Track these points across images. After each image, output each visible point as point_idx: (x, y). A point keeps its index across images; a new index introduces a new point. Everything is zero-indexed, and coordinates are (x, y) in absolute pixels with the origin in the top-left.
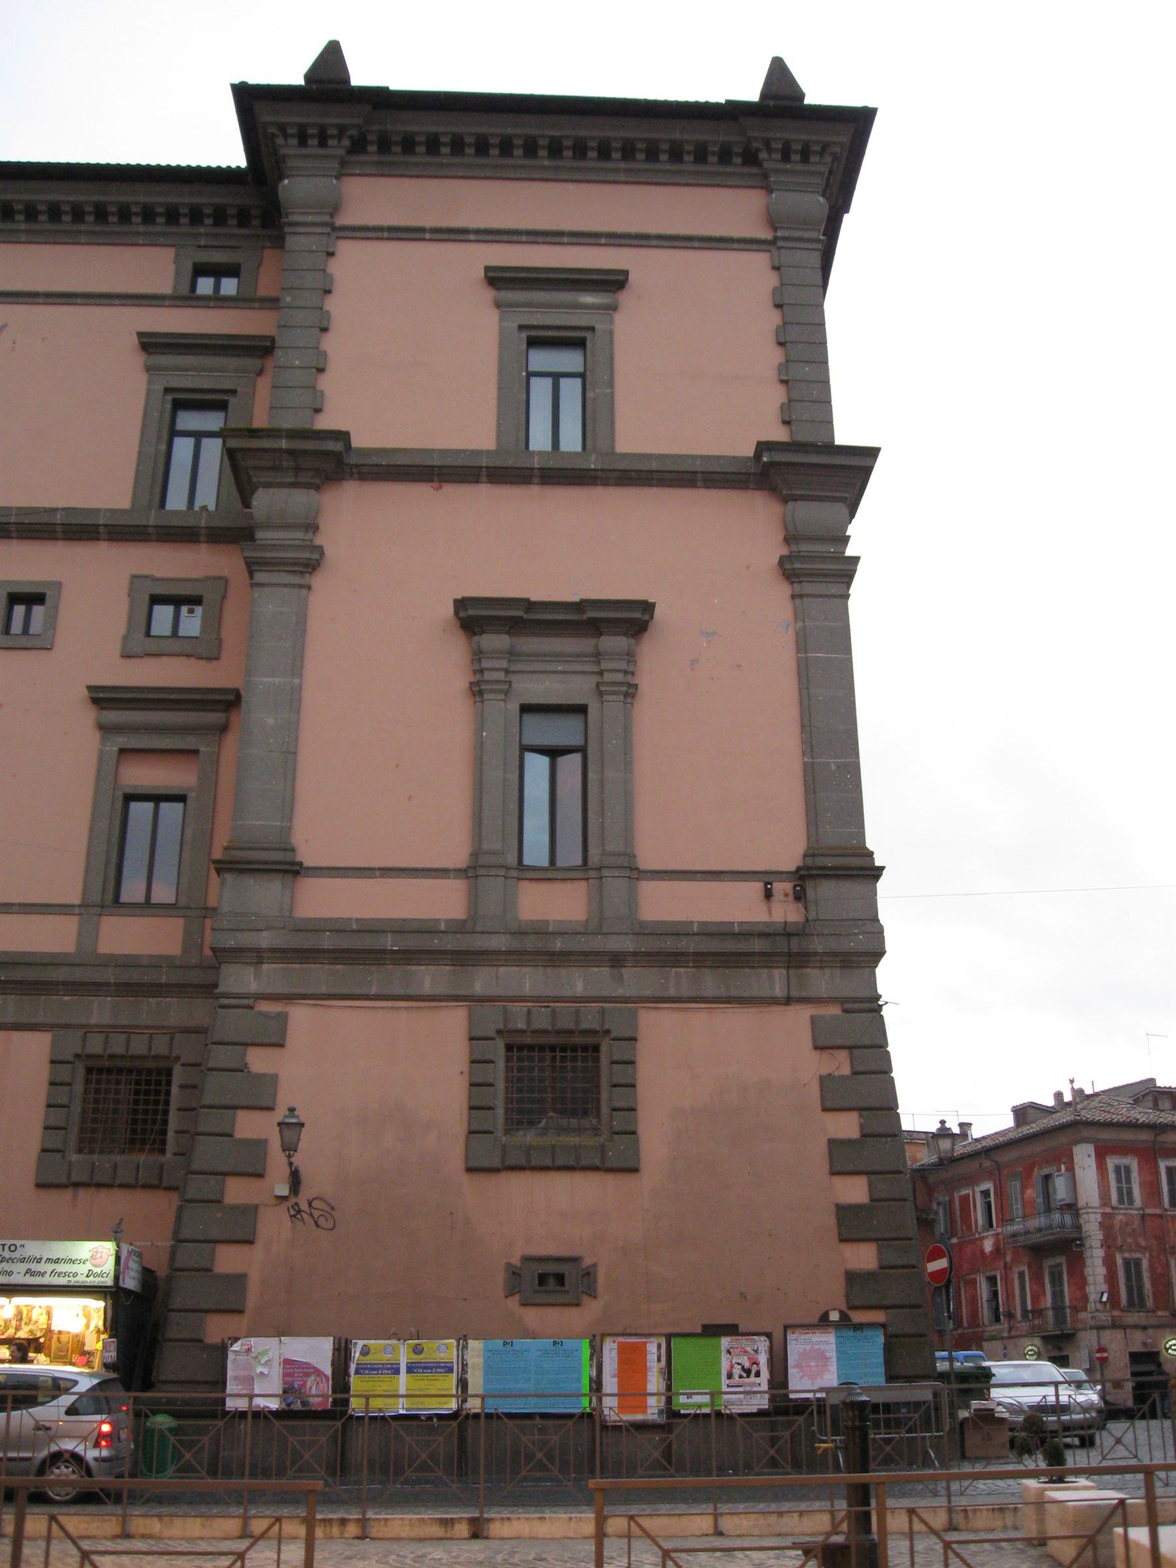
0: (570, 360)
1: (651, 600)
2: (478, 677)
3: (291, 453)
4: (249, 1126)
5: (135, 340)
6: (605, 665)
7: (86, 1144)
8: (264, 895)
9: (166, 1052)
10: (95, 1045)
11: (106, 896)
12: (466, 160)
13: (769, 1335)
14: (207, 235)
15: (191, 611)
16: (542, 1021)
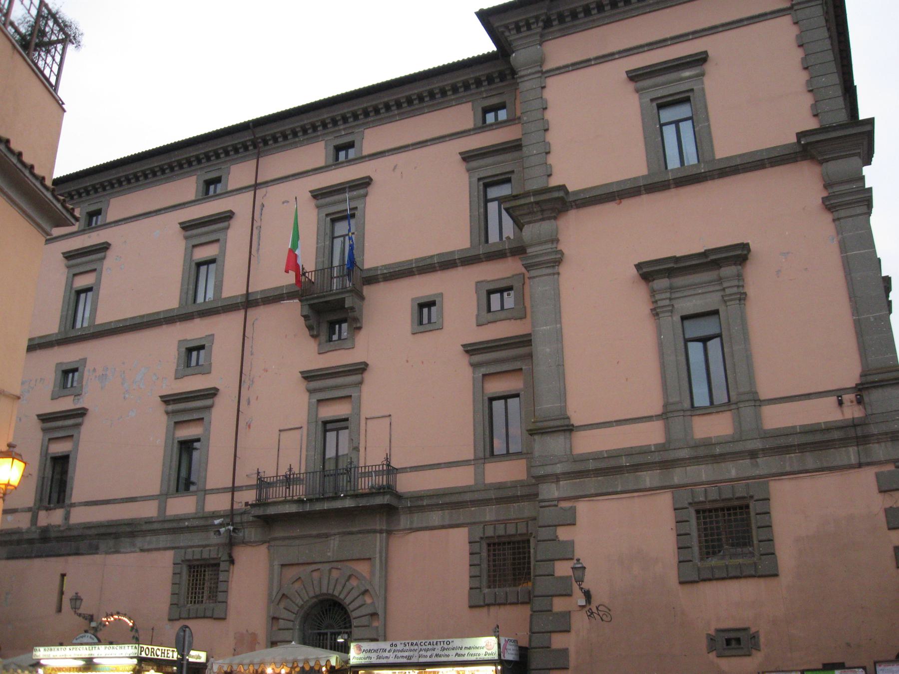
0: (683, 111)
1: (745, 242)
2: (655, 305)
3: (537, 203)
4: (563, 569)
5: (459, 157)
6: (725, 285)
7: (492, 584)
8: (555, 445)
9: (525, 531)
10: (490, 532)
11: (488, 453)
12: (607, 14)
13: (864, 668)
14: (486, 91)
15: (509, 295)
16: (713, 495)
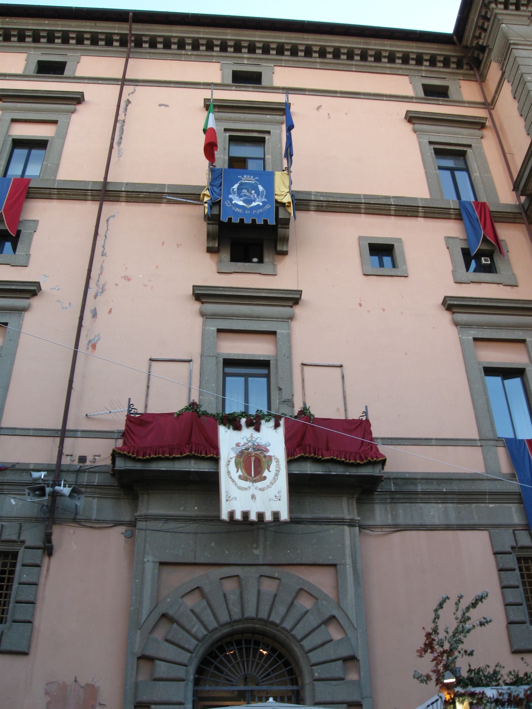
14: (426, 71)
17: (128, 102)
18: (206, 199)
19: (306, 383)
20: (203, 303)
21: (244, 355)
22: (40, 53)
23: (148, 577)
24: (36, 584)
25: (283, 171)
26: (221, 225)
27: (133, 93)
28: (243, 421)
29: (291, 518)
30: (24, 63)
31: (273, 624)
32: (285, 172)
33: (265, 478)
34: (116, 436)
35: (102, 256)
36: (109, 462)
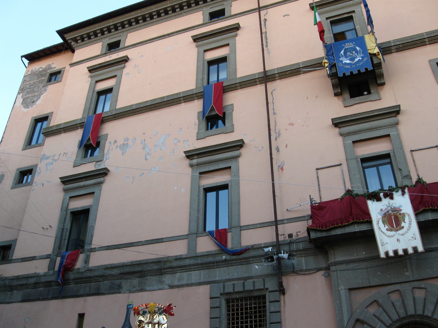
17: (265, 20)
18: (326, 65)
19: (416, 162)
20: (340, 128)
21: (372, 153)
22: (209, 8)
23: (344, 298)
24: (279, 312)
25: (369, 33)
26: (339, 78)
27: (266, 14)
28: (382, 195)
29: (425, 249)
30: (202, 17)
31: (427, 317)
32: (371, 34)
33: (403, 227)
34: (307, 218)
35: (274, 114)
36: (306, 234)
